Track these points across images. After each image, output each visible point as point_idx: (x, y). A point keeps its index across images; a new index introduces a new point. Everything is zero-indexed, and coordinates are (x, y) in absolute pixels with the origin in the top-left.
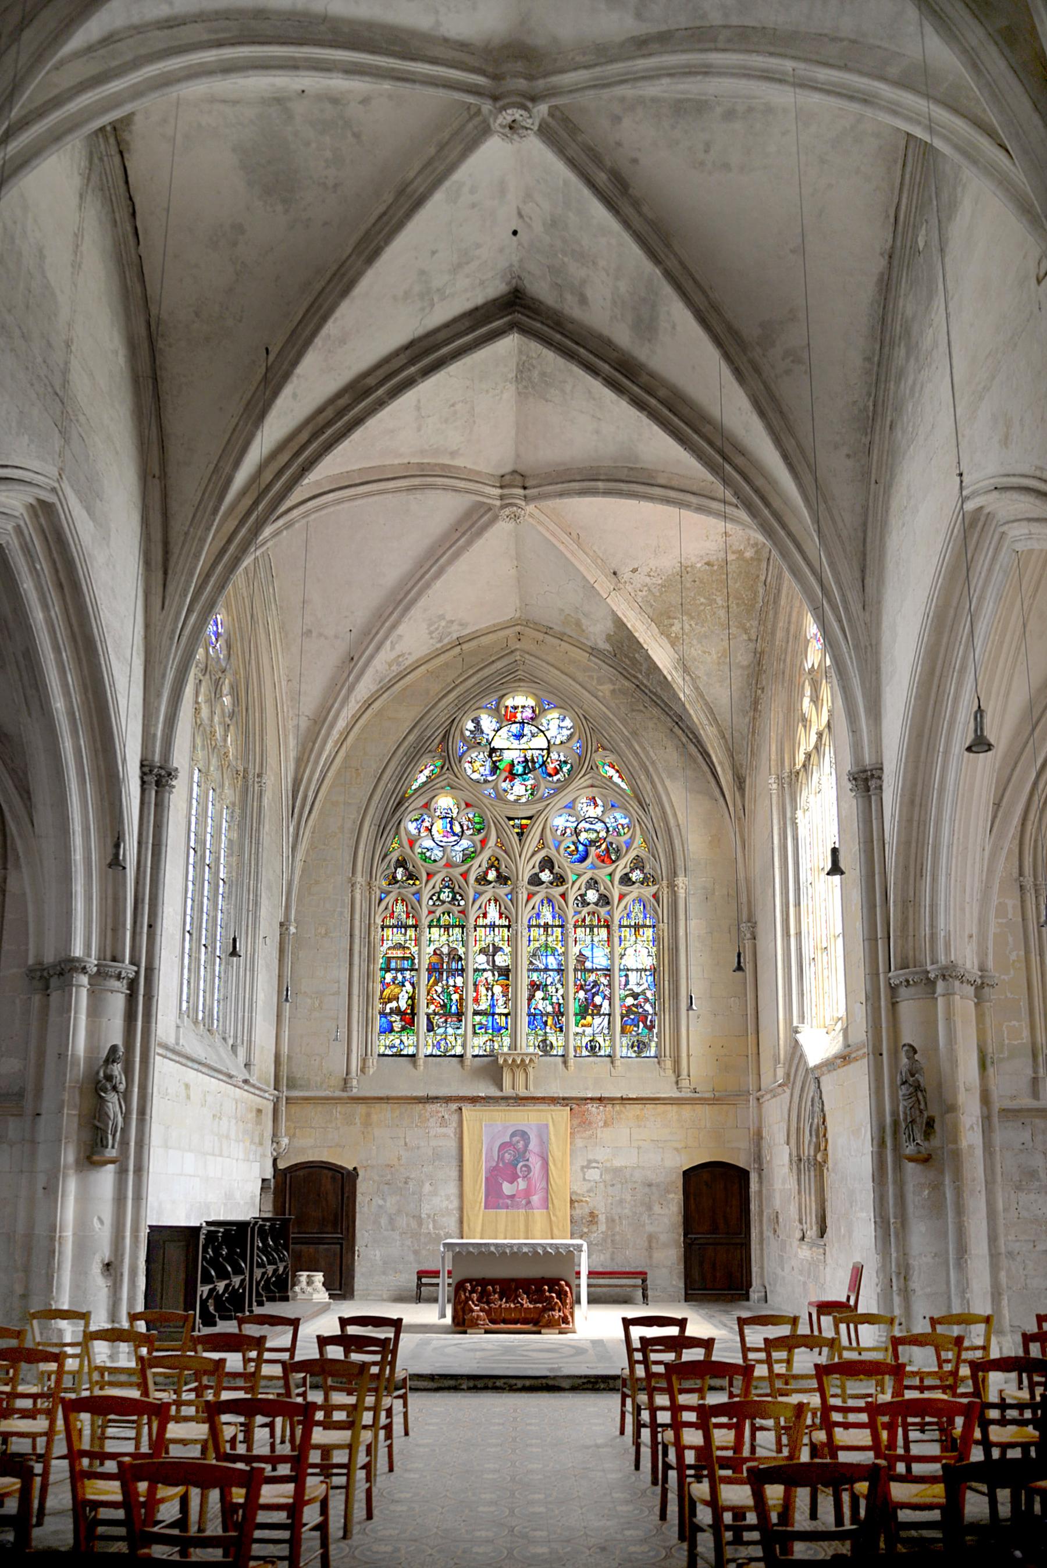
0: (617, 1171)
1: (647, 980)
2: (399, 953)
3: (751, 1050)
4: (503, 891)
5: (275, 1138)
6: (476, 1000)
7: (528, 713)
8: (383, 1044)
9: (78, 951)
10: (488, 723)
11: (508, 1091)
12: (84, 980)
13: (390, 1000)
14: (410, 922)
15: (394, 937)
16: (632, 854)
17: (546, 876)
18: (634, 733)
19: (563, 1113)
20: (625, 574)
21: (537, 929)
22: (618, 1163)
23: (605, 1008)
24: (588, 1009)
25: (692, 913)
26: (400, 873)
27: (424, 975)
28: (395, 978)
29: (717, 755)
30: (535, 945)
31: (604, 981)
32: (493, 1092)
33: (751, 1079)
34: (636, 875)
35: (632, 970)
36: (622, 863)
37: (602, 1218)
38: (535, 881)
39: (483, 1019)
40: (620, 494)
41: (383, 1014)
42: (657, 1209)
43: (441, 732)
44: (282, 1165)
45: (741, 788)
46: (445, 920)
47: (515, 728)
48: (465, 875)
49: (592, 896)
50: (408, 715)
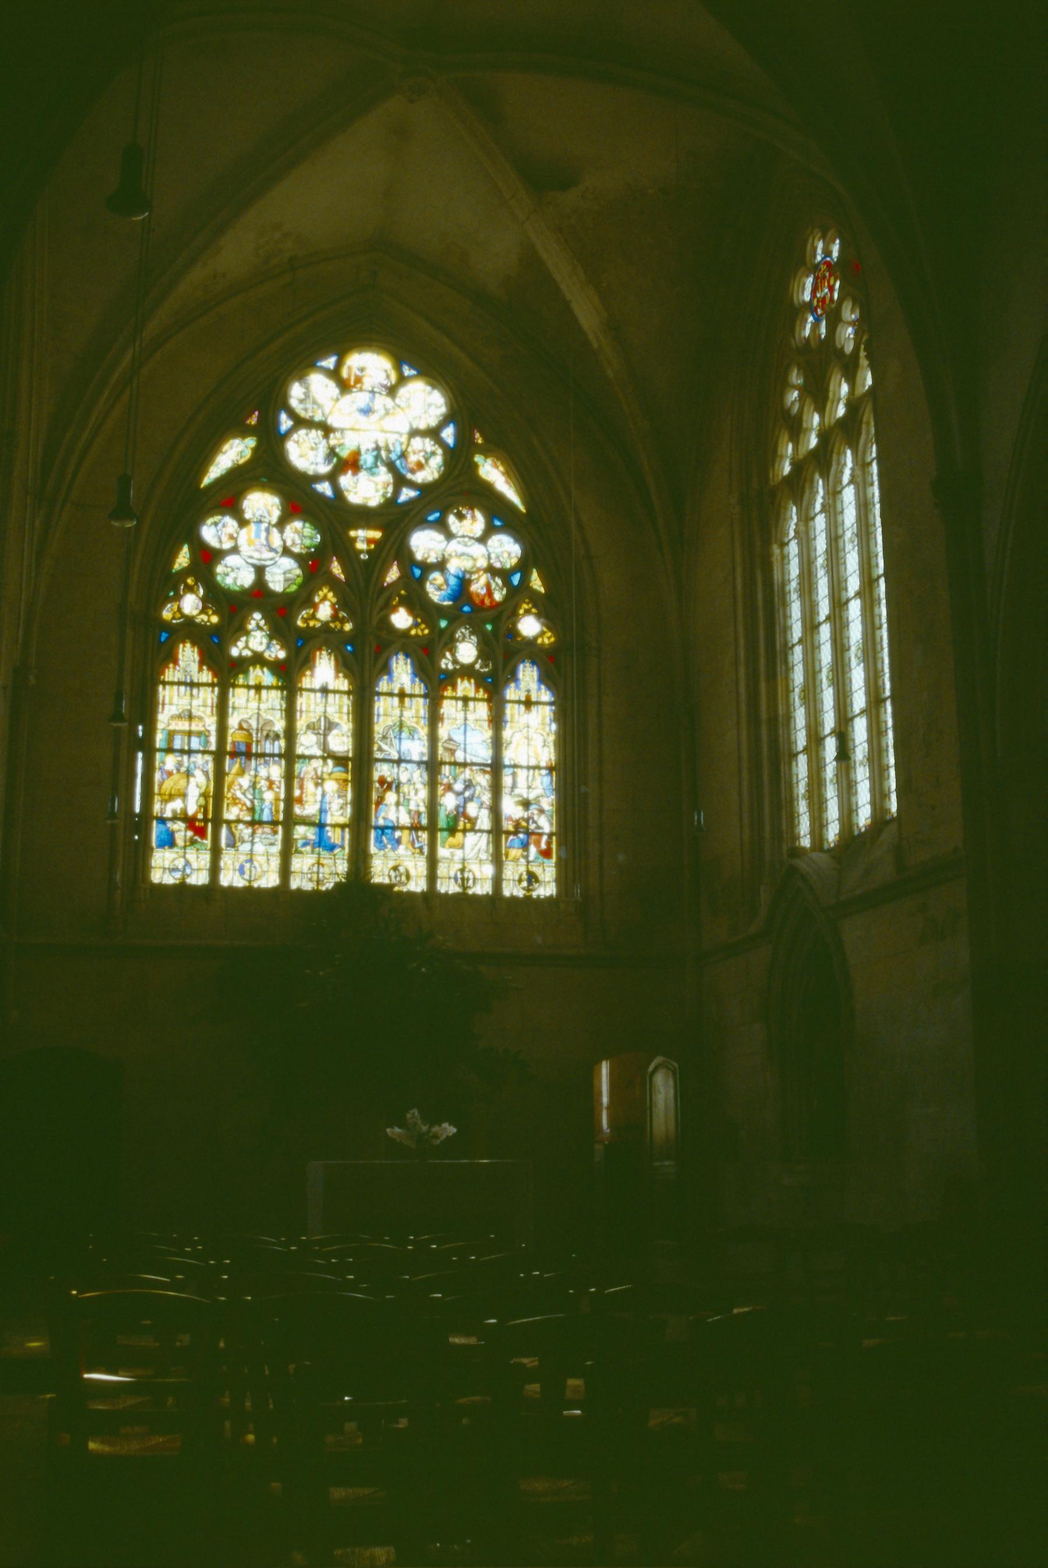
2: (183, 725)
13: (171, 797)
21: (389, 699)
28: (180, 764)
35: (521, 767)
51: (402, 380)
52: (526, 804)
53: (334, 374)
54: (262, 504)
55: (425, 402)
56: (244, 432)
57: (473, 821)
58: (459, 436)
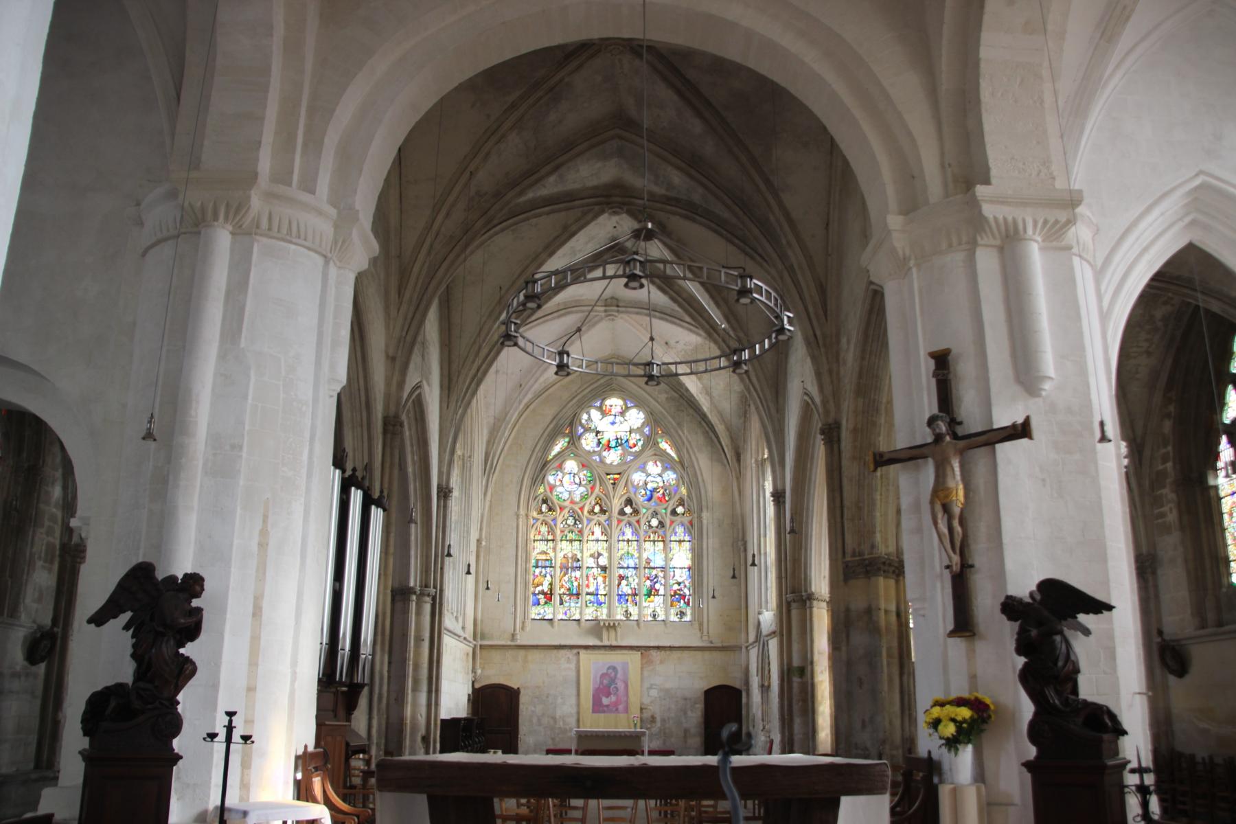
0: (667, 691)
1: (685, 573)
2: (543, 557)
3: (743, 619)
4: (603, 518)
5: (474, 671)
6: (588, 586)
7: (619, 409)
8: (535, 612)
9: (412, 584)
10: (595, 414)
11: (606, 643)
12: (414, 597)
14: (550, 537)
15: (541, 546)
16: (677, 497)
17: (628, 510)
18: (679, 424)
19: (637, 656)
20: (672, 342)
22: (668, 686)
23: (662, 592)
24: (652, 592)
25: (711, 535)
26: (544, 508)
27: (558, 570)
29: (725, 441)
30: (621, 552)
31: (661, 574)
32: (598, 643)
33: (743, 636)
34: (680, 510)
36: (671, 502)
37: (658, 719)
38: (622, 513)
39: (592, 598)
40: (667, 320)
41: (534, 594)
42: (689, 713)
43: (568, 422)
44: (477, 686)
45: (739, 460)
46: (570, 536)
47: (611, 419)
48: (582, 509)
49: (654, 522)
50: (550, 412)
51: (627, 408)
52: (679, 584)
53: (600, 408)
54: (571, 465)
55: (636, 417)
56: (564, 436)
57: (657, 591)
58: (651, 431)
